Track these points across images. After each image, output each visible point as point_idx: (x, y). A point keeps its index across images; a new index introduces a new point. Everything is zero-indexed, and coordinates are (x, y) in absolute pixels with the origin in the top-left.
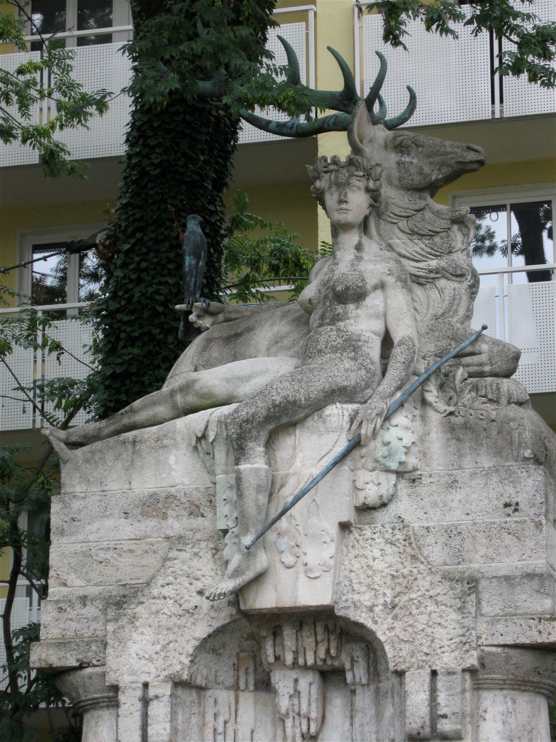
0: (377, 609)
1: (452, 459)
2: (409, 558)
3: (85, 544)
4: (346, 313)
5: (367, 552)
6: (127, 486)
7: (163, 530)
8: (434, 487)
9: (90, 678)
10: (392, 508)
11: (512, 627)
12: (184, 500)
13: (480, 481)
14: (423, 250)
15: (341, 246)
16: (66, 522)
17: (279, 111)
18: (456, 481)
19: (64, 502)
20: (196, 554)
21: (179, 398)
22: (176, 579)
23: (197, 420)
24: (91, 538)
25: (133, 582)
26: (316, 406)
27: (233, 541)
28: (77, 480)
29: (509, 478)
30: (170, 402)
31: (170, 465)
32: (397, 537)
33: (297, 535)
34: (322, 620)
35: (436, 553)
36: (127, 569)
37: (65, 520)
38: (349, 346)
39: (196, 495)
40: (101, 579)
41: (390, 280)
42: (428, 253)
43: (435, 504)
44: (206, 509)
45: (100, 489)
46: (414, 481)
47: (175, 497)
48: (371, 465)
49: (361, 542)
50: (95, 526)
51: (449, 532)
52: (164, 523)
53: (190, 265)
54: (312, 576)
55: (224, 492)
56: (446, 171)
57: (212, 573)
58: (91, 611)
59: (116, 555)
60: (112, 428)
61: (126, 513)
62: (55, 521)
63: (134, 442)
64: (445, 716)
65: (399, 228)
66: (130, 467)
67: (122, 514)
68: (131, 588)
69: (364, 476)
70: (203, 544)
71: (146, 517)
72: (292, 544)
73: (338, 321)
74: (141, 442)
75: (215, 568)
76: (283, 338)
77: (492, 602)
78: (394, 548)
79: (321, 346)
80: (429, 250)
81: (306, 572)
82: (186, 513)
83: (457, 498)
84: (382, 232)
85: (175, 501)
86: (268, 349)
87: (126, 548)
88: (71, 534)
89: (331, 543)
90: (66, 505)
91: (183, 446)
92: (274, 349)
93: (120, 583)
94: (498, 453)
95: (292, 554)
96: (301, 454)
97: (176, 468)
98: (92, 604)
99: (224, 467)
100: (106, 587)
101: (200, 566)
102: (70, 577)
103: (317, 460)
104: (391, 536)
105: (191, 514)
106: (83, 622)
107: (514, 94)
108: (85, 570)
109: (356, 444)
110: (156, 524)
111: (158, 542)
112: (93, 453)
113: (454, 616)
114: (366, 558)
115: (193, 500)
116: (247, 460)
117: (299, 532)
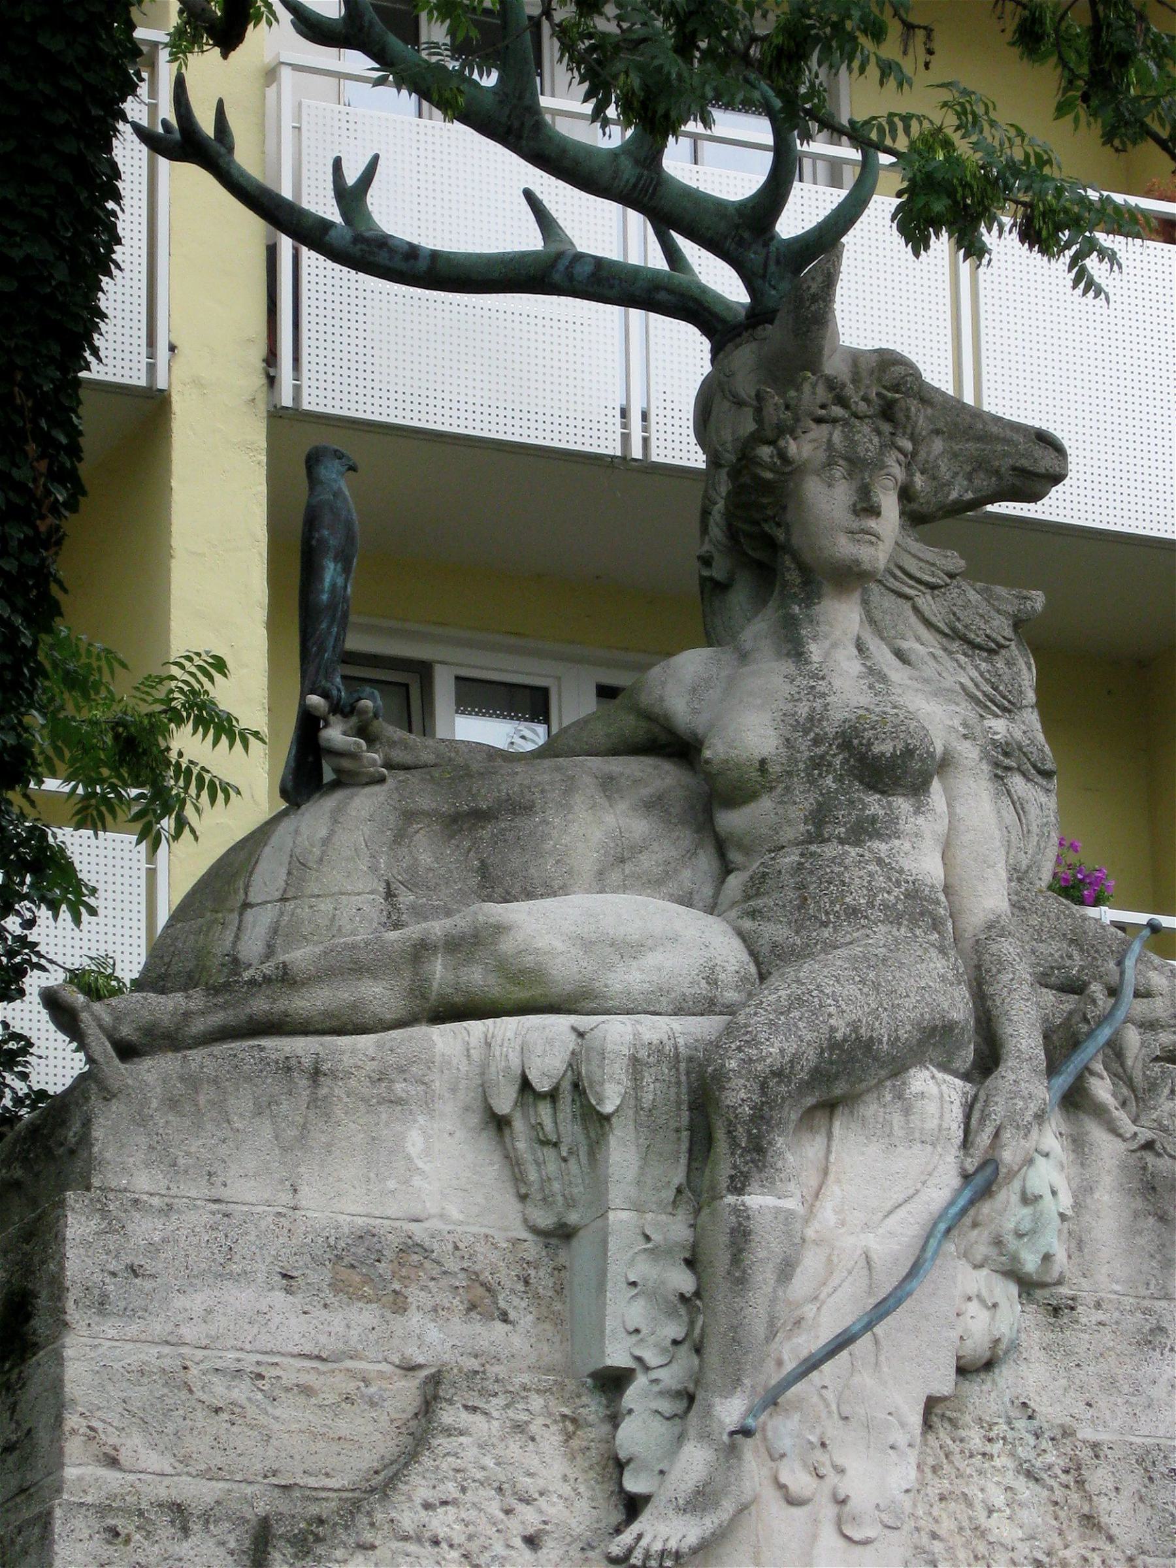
1: (1145, 1268)
2: (1075, 1523)
3: (167, 1350)
4: (895, 820)
5: (972, 1491)
6: (285, 1198)
7: (396, 1342)
8: (1107, 1337)
10: (1005, 1375)
12: (452, 1264)
14: (976, 685)
15: (824, 628)
16: (114, 1274)
17: (1031, 248)
18: (1161, 1329)
19: (104, 1212)
20: (519, 1428)
22: (464, 1490)
23: (540, 1043)
24: (188, 1332)
25: (312, 1482)
27: (654, 1405)
28: (140, 1156)
30: (407, 974)
31: (409, 1158)
32: (1050, 1458)
33: (824, 1415)
37: (111, 1268)
38: (922, 914)
39: (487, 1260)
40: (219, 1460)
41: (969, 752)
42: (985, 694)
44: (516, 1301)
45: (206, 1192)
46: (1056, 1311)
47: (427, 1252)
48: (982, 1250)
49: (957, 1458)
50: (197, 1302)
51: (1148, 1464)
52: (398, 1323)
53: (334, 585)
54: (857, 1536)
55: (631, 1263)
57: (566, 1490)
59: (260, 1396)
60: (217, 1019)
61: (285, 1276)
65: (916, 610)
66: (295, 1145)
67: (278, 1278)
68: (308, 1498)
70: (536, 1402)
71: (345, 1298)
72: (813, 1439)
73: (871, 838)
74: (333, 1074)
75: (571, 1476)
76: (636, 850)
78: (1037, 1488)
80: (988, 689)
81: (839, 1523)
83: (1165, 1377)
84: (877, 615)
85: (428, 1264)
86: (601, 874)
87: (289, 1378)
88: (129, 1313)
89: (909, 1451)
90: (113, 1227)
91: (449, 1107)
92: (615, 876)
93: (275, 1481)
95: (805, 1465)
96: (836, 1189)
97: (426, 1168)
98: (207, 1530)
99: (633, 1192)
100: (235, 1486)
101: (533, 1462)
102: (129, 1443)
103: (880, 1215)
104: (1033, 1454)
105: (472, 1307)
107: (1019, 313)
108: (170, 1428)
110: (375, 1322)
111: (381, 1375)
112: (193, 1082)
114: (970, 1504)
115: (477, 1268)
116: (769, 1186)
117: (827, 1406)
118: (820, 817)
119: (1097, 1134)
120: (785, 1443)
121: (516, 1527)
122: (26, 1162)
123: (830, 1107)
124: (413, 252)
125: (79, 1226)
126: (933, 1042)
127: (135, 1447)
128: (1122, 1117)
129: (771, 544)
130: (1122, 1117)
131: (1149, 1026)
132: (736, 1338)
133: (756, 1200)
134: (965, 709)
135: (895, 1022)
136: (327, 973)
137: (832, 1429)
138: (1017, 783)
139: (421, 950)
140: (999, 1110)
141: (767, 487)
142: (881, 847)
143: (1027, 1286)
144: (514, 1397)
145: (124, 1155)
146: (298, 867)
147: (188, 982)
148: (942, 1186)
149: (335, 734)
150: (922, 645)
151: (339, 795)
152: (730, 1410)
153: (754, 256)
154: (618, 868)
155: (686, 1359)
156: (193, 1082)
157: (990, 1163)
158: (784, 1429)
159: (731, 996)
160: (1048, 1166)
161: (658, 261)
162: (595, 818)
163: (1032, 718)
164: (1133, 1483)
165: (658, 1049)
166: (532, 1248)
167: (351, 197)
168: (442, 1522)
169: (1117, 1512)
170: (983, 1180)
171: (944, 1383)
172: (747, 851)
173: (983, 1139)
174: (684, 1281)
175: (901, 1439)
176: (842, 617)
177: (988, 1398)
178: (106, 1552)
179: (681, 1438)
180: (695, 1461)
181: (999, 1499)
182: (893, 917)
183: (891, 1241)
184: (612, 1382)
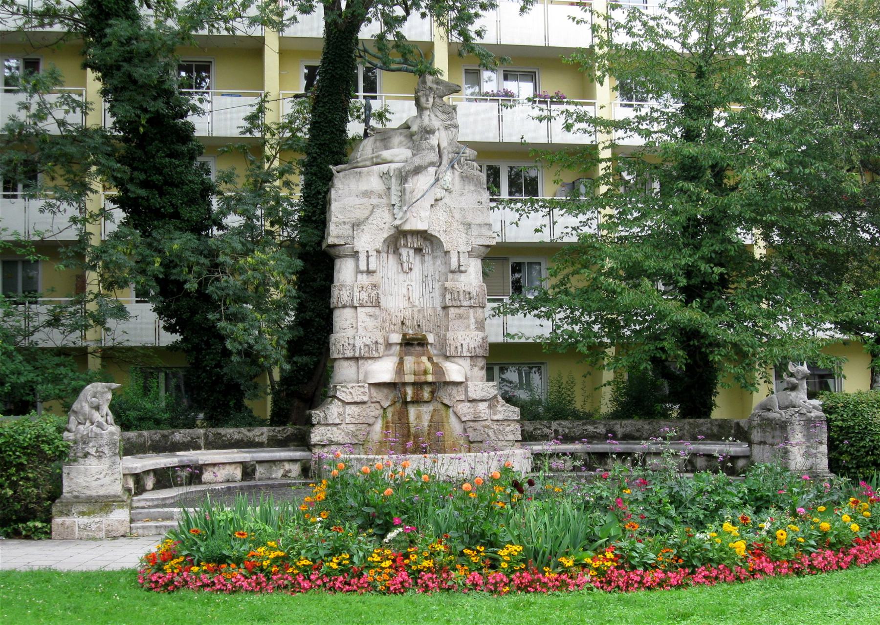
13: (470, 194)
23: (384, 168)
26: (426, 167)
29: (479, 193)
34: (424, 235)
35: (457, 215)
36: (360, 214)
39: (380, 192)
41: (441, 128)
58: (347, 227)
62: (333, 196)
66: (358, 181)
69: (437, 190)
77: (475, 231)
90: (337, 192)
94: (476, 186)
106: (346, 230)
109: (437, 180)
125: (333, 192)
126: (432, 164)
127: (339, 216)
133: (406, 185)
136: (362, 161)
148: (433, 180)
158: (413, 209)
171: (433, 203)
180: (401, 214)
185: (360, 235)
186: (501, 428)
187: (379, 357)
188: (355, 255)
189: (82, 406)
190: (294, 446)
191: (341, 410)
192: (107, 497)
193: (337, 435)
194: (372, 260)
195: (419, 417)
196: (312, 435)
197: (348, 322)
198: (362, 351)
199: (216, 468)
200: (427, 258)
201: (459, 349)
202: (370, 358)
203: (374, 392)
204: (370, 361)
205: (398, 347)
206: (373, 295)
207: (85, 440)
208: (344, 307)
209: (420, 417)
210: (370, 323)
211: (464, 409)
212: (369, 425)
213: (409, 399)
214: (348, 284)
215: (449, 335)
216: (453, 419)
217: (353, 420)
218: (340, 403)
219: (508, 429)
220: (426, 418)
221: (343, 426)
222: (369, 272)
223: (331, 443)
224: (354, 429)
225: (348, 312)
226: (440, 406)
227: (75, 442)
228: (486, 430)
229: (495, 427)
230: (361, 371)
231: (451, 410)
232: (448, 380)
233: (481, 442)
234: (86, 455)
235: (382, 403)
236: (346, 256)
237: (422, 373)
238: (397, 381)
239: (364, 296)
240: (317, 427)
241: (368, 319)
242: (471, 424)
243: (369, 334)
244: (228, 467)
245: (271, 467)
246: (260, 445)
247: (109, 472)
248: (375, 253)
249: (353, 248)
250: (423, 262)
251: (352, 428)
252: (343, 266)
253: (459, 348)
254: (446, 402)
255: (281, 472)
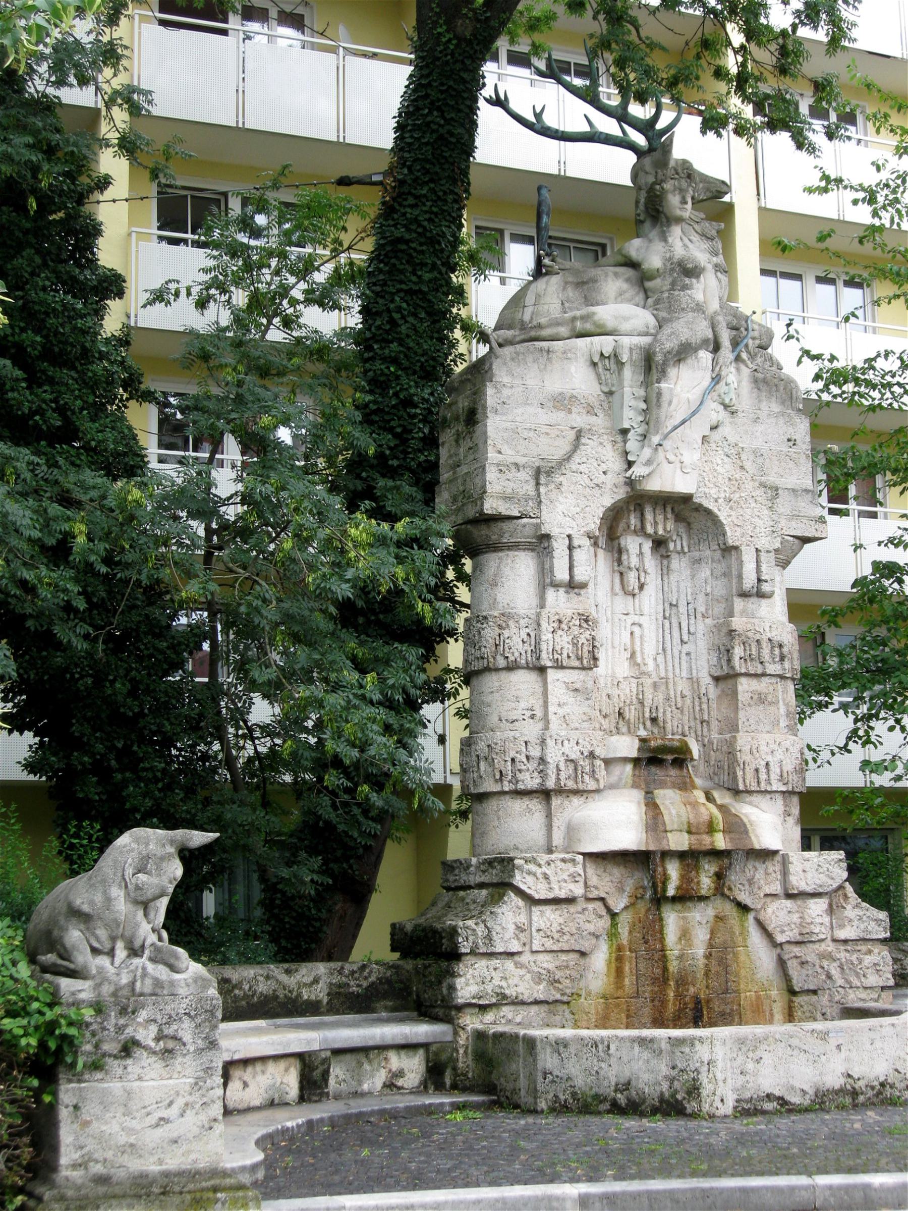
0: (720, 501)
9: (524, 526)
10: (720, 429)
11: (801, 525)
13: (773, 420)
20: (601, 443)
21: (578, 324)
23: (605, 344)
24: (518, 419)
29: (790, 422)
34: (681, 506)
36: (556, 449)
39: (592, 400)
41: (709, 267)
43: (746, 432)
48: (716, 398)
50: (519, 411)
56: (709, 195)
60: (522, 337)
63: (548, 351)
64: (766, 581)
70: (605, 437)
77: (784, 504)
79: (684, 306)
82: (584, 411)
94: (783, 403)
112: (517, 354)
113: (766, 512)
118: (673, 284)
119: (742, 367)
120: (668, 448)
121: (601, 469)
122: (472, 374)
123: (679, 361)
124: (557, 131)
125: (490, 391)
126: (705, 342)
127: (505, 449)
128: (749, 363)
129: (658, 211)
130: (749, 363)
131: (753, 339)
132: (657, 421)
133: (663, 385)
134: (708, 255)
135: (695, 340)
137: (680, 444)
138: (719, 274)
139: (574, 319)
140: (721, 361)
141: (658, 196)
142: (689, 292)
143: (726, 406)
144: (600, 436)
145: (501, 373)
146: (538, 296)
147: (510, 327)
148: (707, 381)
149: (546, 261)
150: (695, 238)
151: (546, 278)
152: (656, 439)
153: (650, 134)
154: (620, 297)
155: (644, 426)
156: (517, 354)
157: (719, 375)
158: (667, 444)
159: (653, 331)
160: (731, 375)
161: (620, 134)
162: (613, 283)
163: (721, 256)
164: (752, 457)
165: (636, 346)
166: (603, 397)
167: (538, 116)
168: (582, 468)
169: (748, 465)
170: (717, 379)
171: (707, 432)
172: (654, 292)
173: (717, 369)
174: (644, 406)
175: (696, 446)
176: (676, 231)
177: (716, 436)
178: (499, 475)
179: (643, 447)
181: (720, 462)
182: (693, 310)
183: (694, 395)
184: (624, 432)
185: (553, 495)
186: (854, 958)
187: (597, 791)
188: (541, 543)
189: (108, 900)
190: (387, 1009)
191: (522, 919)
192: (193, 1175)
193: (518, 981)
194: (580, 556)
195: (685, 935)
196: (459, 982)
197: (523, 705)
198: (563, 776)
199: (250, 1069)
200: (675, 563)
201: (763, 776)
202: (576, 792)
203: (592, 872)
204: (576, 801)
205: (629, 767)
206: (582, 640)
207: (127, 1004)
208: (512, 667)
209: (688, 932)
210: (575, 708)
211: (779, 914)
212: (583, 954)
213: (671, 892)
214: (522, 612)
215: (743, 741)
216: (755, 938)
217: (549, 945)
218: (521, 903)
219: (868, 960)
220: (701, 937)
221: (526, 958)
222: (573, 586)
223: (503, 1000)
224: (551, 966)
225: (523, 683)
226: (729, 909)
227: (99, 1008)
228: (825, 963)
229: (842, 955)
230: (556, 823)
231: (751, 916)
232: (757, 847)
233: (815, 992)
234: (128, 1049)
235: (611, 902)
236: (515, 546)
237: (704, 828)
238: (652, 848)
239: (563, 641)
240: (469, 960)
241: (569, 698)
242: (796, 950)
243: (574, 735)
244: (271, 1067)
245: (360, 1064)
246: (312, 1008)
247: (196, 1097)
248: (586, 542)
249: (538, 526)
250: (665, 571)
251: (547, 962)
252: (506, 571)
253: (763, 770)
254: (744, 897)
255: (380, 1078)
